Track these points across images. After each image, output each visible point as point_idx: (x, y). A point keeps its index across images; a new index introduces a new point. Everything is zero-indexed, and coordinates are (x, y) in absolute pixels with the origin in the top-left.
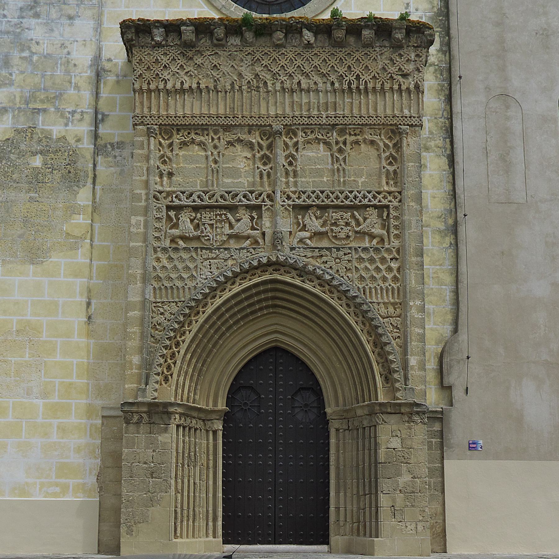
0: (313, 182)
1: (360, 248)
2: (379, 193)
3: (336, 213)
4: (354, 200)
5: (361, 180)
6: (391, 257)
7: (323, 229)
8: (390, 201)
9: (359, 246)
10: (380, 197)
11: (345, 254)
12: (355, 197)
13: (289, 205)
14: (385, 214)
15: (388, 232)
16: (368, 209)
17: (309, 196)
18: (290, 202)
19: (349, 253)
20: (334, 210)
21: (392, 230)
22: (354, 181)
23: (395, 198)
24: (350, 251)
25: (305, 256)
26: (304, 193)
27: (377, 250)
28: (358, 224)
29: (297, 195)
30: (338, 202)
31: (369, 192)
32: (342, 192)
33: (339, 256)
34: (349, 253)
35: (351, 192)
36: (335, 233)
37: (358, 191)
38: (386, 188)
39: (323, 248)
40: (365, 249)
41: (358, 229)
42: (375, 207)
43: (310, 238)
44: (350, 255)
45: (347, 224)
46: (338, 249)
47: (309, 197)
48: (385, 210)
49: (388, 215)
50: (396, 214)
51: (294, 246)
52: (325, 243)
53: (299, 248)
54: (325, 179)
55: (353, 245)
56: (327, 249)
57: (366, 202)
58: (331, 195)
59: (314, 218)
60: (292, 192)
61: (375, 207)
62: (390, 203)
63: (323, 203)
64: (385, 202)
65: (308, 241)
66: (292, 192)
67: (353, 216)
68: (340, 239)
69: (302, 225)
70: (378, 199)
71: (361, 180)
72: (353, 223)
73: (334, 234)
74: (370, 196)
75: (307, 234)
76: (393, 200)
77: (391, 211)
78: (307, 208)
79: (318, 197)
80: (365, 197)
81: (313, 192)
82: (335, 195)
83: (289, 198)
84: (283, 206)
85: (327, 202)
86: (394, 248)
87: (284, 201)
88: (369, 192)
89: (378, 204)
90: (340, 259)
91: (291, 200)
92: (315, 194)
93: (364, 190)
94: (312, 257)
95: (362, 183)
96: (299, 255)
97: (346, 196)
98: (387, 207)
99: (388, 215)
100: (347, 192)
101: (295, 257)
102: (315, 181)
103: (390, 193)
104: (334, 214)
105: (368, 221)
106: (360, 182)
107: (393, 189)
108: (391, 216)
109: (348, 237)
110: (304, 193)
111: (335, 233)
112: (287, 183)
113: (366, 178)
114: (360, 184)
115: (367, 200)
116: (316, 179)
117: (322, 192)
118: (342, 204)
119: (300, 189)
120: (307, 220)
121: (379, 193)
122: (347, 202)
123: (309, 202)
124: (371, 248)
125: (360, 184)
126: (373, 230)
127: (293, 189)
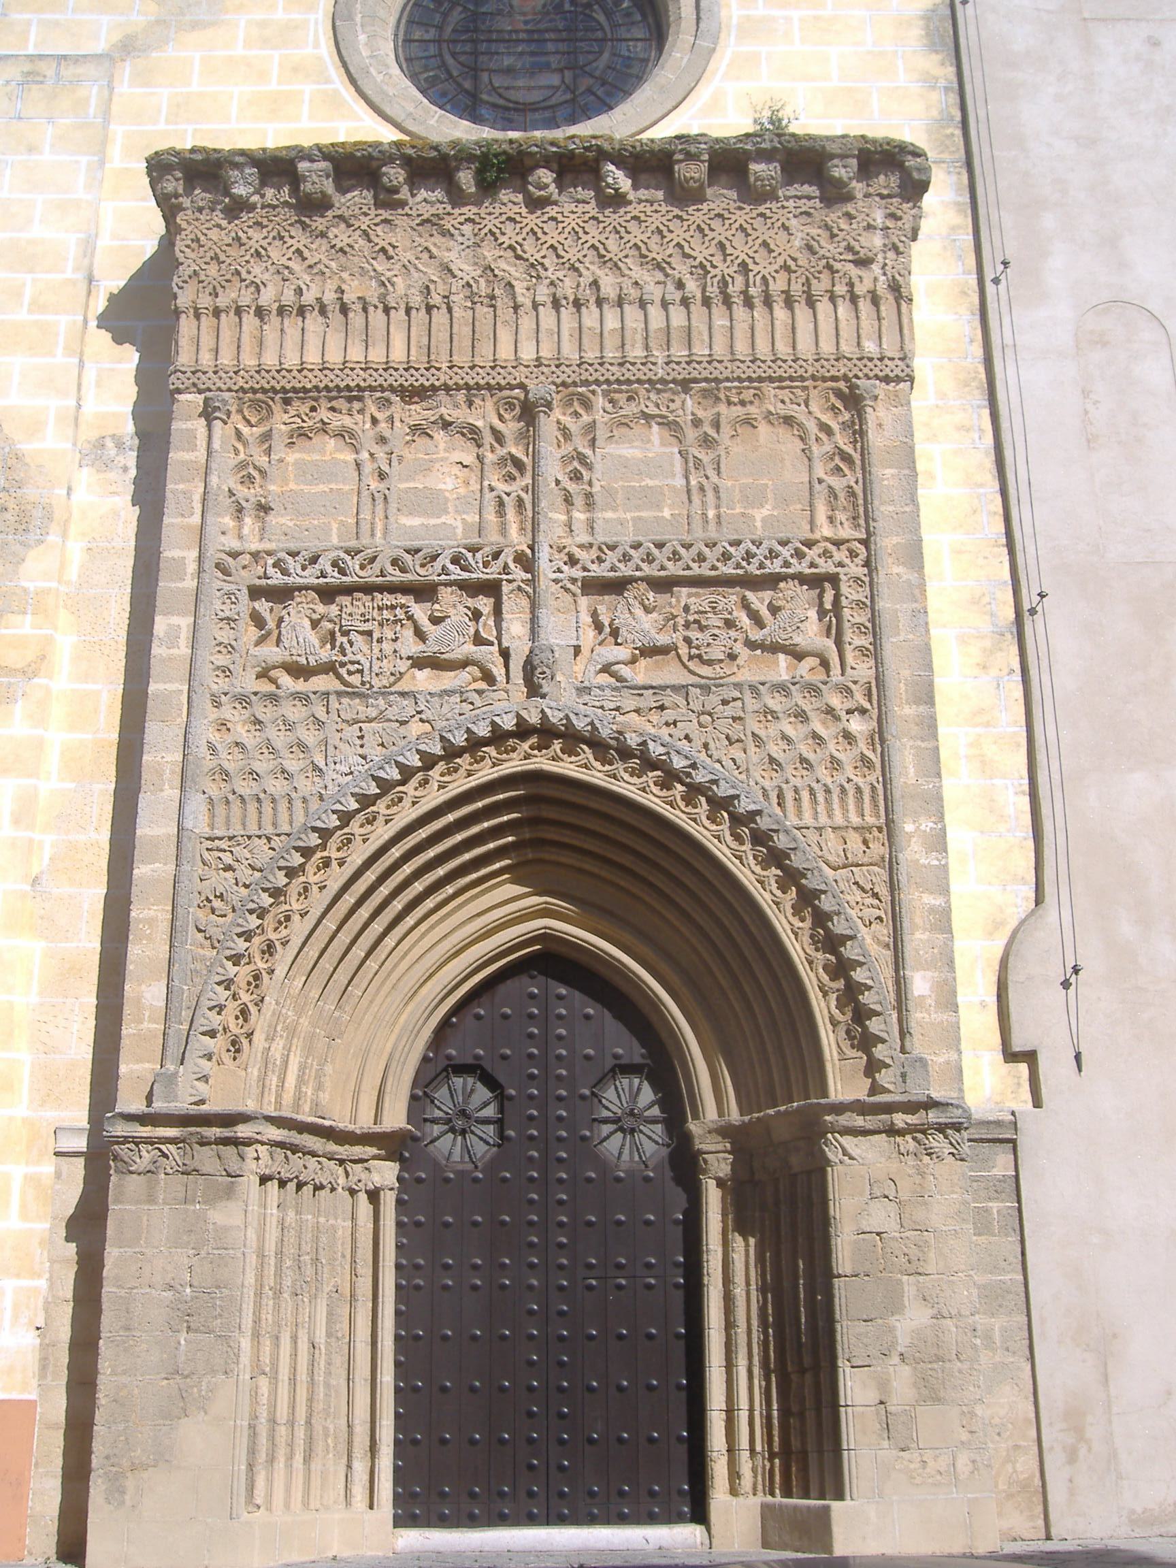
0: (633, 519)
1: (763, 684)
2: (810, 544)
3: (697, 595)
4: (744, 563)
5: (759, 514)
6: (850, 705)
7: (663, 639)
8: (841, 565)
9: (762, 679)
10: (811, 554)
11: (725, 702)
12: (749, 556)
13: (573, 581)
14: (829, 596)
15: (839, 643)
16: (782, 585)
17: (624, 555)
18: (577, 573)
19: (734, 700)
20: (694, 590)
21: (848, 635)
22: (743, 515)
23: (853, 554)
24: (737, 694)
25: (617, 709)
26: (612, 548)
27: (813, 690)
28: (758, 622)
29: (594, 553)
30: (705, 571)
31: (784, 543)
32: (712, 545)
33: (708, 708)
34: (734, 700)
35: (736, 543)
36: (698, 648)
37: (753, 542)
38: (827, 531)
39: (663, 688)
40: (781, 688)
41: (756, 635)
42: (802, 579)
43: (633, 661)
44: (739, 703)
45: (730, 624)
46: (706, 689)
47: (626, 558)
48: (827, 585)
49: (837, 597)
50: (855, 597)
51: (586, 684)
52: (670, 673)
53: (600, 688)
54: (666, 513)
55: (745, 675)
56: (675, 688)
57: (775, 567)
58: (683, 551)
59: (639, 611)
60: (581, 546)
61: (802, 579)
62: (839, 569)
63: (663, 573)
64: (826, 567)
65: (625, 671)
66: (581, 546)
67: (746, 605)
68: (709, 663)
69: (607, 630)
70: (808, 558)
71: (759, 514)
72: (744, 620)
73: (694, 651)
74: (786, 552)
75: (623, 653)
76: (847, 561)
77: (844, 589)
78: (616, 586)
79: (649, 559)
80: (773, 555)
81: (637, 546)
82: (694, 551)
83: (572, 561)
84: (556, 581)
85: (674, 569)
86: (855, 682)
87: (559, 571)
88: (784, 543)
89: (758, 572)
90: (710, 714)
91: (579, 566)
92: (641, 550)
93: (769, 538)
94: (637, 711)
95: (764, 520)
96: (602, 707)
97: (723, 554)
98: (834, 579)
99: (837, 597)
100: (726, 545)
101: (589, 711)
102: (640, 518)
103: (838, 543)
104: (693, 600)
105: (783, 614)
106: (758, 517)
107: (846, 532)
108: (844, 602)
109: (732, 657)
110: (612, 548)
111: (698, 648)
112: (569, 525)
113: (774, 508)
114: (758, 524)
115: (778, 563)
116: (644, 514)
117: (660, 546)
118: (713, 573)
119: (601, 539)
120: (622, 618)
121: (810, 544)
122: (728, 570)
123: (625, 570)
124: (794, 684)
125: (758, 524)
126: (798, 639)
127: (584, 538)
